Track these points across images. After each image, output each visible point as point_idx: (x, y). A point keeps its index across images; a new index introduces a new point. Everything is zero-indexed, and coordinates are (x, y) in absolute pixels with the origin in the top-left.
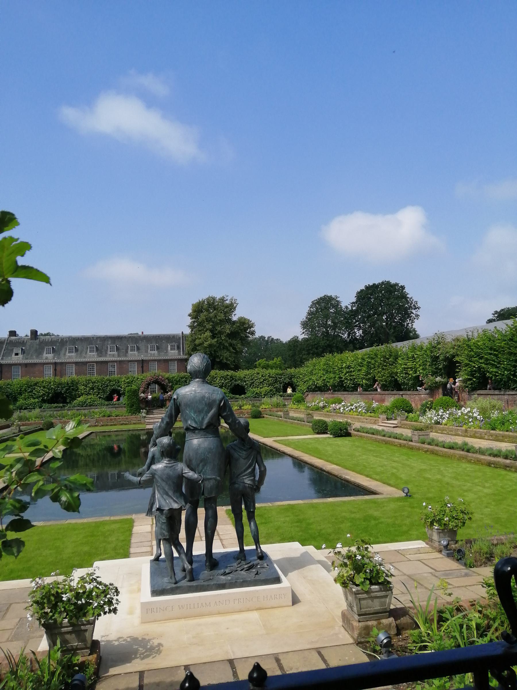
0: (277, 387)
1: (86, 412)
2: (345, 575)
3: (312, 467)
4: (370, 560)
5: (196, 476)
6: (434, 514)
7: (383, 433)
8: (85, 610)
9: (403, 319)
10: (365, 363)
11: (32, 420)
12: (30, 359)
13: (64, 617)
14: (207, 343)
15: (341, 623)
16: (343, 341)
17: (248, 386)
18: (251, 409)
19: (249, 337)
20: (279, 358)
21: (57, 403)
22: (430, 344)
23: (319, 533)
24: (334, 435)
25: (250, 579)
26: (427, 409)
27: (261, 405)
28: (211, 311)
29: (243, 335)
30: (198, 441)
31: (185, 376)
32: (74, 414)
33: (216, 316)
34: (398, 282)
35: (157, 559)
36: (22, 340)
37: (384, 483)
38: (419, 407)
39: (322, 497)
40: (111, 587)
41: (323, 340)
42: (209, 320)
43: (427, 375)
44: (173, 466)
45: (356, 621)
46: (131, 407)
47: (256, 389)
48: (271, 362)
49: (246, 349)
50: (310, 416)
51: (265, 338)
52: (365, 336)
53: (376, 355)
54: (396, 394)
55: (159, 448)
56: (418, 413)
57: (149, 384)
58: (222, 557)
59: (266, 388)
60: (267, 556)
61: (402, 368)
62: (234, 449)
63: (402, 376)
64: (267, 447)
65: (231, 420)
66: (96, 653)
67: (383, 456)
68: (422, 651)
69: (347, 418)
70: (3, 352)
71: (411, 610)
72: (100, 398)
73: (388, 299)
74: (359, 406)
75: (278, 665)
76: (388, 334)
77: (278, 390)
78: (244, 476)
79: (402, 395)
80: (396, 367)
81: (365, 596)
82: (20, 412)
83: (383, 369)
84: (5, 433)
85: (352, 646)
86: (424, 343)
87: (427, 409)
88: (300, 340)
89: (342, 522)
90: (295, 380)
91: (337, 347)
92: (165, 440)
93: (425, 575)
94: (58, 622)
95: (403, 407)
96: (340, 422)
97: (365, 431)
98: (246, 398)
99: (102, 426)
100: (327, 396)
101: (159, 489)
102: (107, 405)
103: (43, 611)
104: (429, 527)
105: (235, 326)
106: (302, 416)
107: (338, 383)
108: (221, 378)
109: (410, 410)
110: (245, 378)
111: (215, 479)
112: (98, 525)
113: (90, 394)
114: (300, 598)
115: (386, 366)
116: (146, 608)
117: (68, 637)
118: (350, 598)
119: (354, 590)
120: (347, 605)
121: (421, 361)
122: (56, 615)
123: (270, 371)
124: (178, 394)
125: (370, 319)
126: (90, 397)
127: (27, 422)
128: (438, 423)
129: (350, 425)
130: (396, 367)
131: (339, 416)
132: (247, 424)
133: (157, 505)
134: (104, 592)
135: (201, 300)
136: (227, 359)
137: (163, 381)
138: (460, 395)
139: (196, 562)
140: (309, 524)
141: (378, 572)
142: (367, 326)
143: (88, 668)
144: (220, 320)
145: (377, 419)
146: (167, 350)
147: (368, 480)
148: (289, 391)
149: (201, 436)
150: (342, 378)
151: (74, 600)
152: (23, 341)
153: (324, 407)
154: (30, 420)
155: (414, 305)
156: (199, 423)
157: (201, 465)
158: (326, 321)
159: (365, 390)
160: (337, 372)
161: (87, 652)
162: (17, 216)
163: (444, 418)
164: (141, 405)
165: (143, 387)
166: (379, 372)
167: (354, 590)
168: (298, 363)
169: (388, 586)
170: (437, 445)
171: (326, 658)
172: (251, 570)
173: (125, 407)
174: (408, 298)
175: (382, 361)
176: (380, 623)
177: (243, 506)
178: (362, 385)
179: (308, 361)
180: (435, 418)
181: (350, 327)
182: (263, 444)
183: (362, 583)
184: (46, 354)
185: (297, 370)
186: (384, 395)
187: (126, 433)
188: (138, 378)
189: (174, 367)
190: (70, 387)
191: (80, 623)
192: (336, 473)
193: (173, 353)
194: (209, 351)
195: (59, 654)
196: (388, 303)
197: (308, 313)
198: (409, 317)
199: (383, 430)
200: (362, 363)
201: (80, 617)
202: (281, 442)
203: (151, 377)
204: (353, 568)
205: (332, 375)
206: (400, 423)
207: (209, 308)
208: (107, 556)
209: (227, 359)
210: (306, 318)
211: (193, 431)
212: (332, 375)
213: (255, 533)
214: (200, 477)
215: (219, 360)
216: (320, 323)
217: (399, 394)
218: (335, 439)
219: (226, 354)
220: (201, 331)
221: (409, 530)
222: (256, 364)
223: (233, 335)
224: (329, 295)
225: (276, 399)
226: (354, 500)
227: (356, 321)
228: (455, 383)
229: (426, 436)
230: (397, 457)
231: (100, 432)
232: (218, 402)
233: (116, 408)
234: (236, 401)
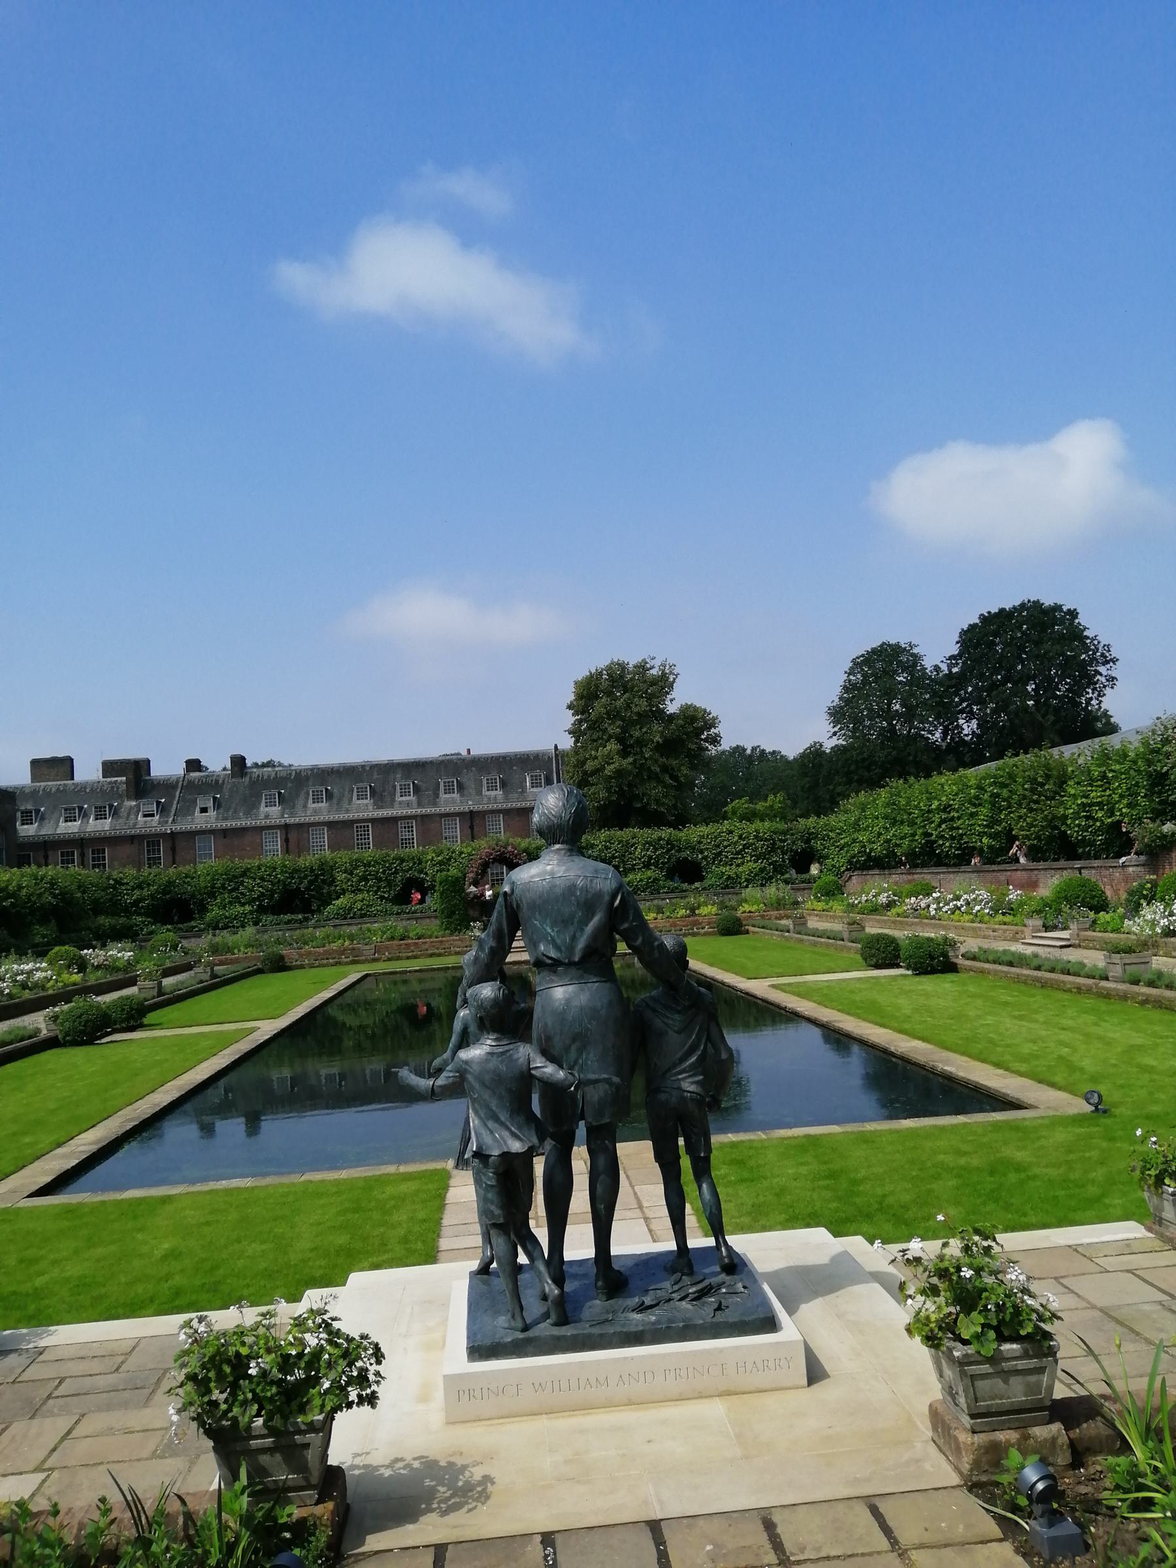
0: (776, 861)
1: (354, 929)
2: (933, 1317)
4: (997, 1279)
5: (561, 1074)
6: (1164, 1156)
7: (1035, 963)
8: (303, 1398)
9: (1077, 689)
10: (986, 796)
11: (239, 951)
12: (233, 818)
13: (254, 1413)
14: (612, 766)
15: (929, 1434)
16: (931, 747)
17: (708, 862)
20: (780, 797)
21: (292, 913)
22: (1145, 743)
23: (880, 1203)
24: (914, 969)
25: (701, 1322)
26: (1142, 901)
27: (740, 903)
28: (618, 694)
29: (694, 747)
30: (565, 992)
32: (328, 936)
33: (628, 707)
37: (1040, 1082)
38: (1124, 896)
39: (891, 1117)
40: (365, 1343)
41: (882, 749)
43: (1140, 819)
44: (507, 1051)
45: (965, 1429)
46: (449, 917)
47: (728, 868)
48: (760, 806)
50: (855, 926)
52: (983, 734)
54: (1066, 869)
55: (473, 1010)
56: (1121, 910)
58: (637, 1265)
59: (750, 866)
61: (1078, 805)
62: (654, 1010)
63: (1079, 825)
65: (640, 940)
66: (331, 1498)
67: (1037, 1016)
68: (1140, 1511)
69: (944, 927)
70: (174, 806)
71: (1107, 1404)
72: (382, 898)
74: (975, 899)
75: (770, 1540)
78: (680, 1073)
79: (1080, 869)
81: (986, 1368)
82: (214, 935)
83: (1031, 810)
84: (182, 983)
85: (957, 1492)
86: (1130, 743)
87: (1142, 901)
88: (828, 751)
89: (937, 1177)
90: (818, 845)
92: (487, 991)
93: (1147, 1307)
94: (241, 1425)
95: (1083, 899)
96: (930, 939)
97: (991, 958)
98: (704, 889)
99: (389, 959)
100: (897, 878)
102: (398, 914)
103: (206, 1399)
104: (1152, 1189)
105: (673, 726)
106: (837, 926)
108: (644, 845)
109: (1102, 905)
110: (700, 842)
111: (607, 1081)
112: (370, 1184)
113: (360, 890)
114: (828, 1366)
116: (457, 1387)
117: (264, 1459)
118: (948, 1373)
119: (956, 1354)
120: (943, 1388)
122: (236, 1410)
123: (757, 824)
124: (513, 883)
125: (994, 693)
126: (360, 896)
127: (229, 956)
129: (953, 944)
130: (1062, 803)
131: (927, 925)
134: (346, 1354)
135: (593, 671)
136: (657, 801)
137: (516, 856)
139: (575, 1276)
140: (855, 1182)
141: (1017, 1311)
142: (988, 711)
143: (314, 1534)
144: (638, 714)
145: (1020, 928)
146: (524, 791)
149: (571, 980)
150: (931, 835)
151: (276, 1374)
152: (217, 781)
153: (890, 905)
154: (236, 951)
155: (1103, 655)
157: (574, 1048)
158: (889, 704)
159: (990, 861)
160: (918, 821)
161: (310, 1496)
164: (471, 913)
166: (1020, 817)
167: (956, 1354)
168: (824, 805)
169: (1046, 1344)
171: (890, 1523)
172: (704, 1299)
173: (436, 917)
174: (1087, 638)
175: (1026, 790)
176: (1026, 1437)
177: (681, 1141)
178: (981, 849)
179: (848, 800)
181: (946, 714)
182: (747, 994)
183: (978, 1337)
184: (266, 806)
185: (823, 820)
186: (1036, 872)
187: (442, 974)
188: (461, 853)
190: (317, 876)
191: (291, 1429)
192: (921, 1059)
194: (616, 786)
195: (245, 1499)
197: (845, 687)
198: (1091, 682)
199: (1036, 956)
200: (977, 797)
201: (291, 1413)
202: (787, 989)
204: (954, 1301)
205: (907, 830)
206: (1078, 935)
208: (385, 1257)
209: (657, 801)
212: (907, 830)
213: (714, 1210)
214: (570, 1077)
215: (639, 805)
216: (873, 710)
217: (1072, 868)
218: (918, 979)
219: (656, 791)
221: (1103, 1195)
222: (726, 812)
223: (670, 747)
224: (893, 642)
226: (965, 1125)
227: (962, 700)
230: (1072, 1018)
231: (384, 974)
232: (607, 898)
233: (416, 919)
234: (682, 898)
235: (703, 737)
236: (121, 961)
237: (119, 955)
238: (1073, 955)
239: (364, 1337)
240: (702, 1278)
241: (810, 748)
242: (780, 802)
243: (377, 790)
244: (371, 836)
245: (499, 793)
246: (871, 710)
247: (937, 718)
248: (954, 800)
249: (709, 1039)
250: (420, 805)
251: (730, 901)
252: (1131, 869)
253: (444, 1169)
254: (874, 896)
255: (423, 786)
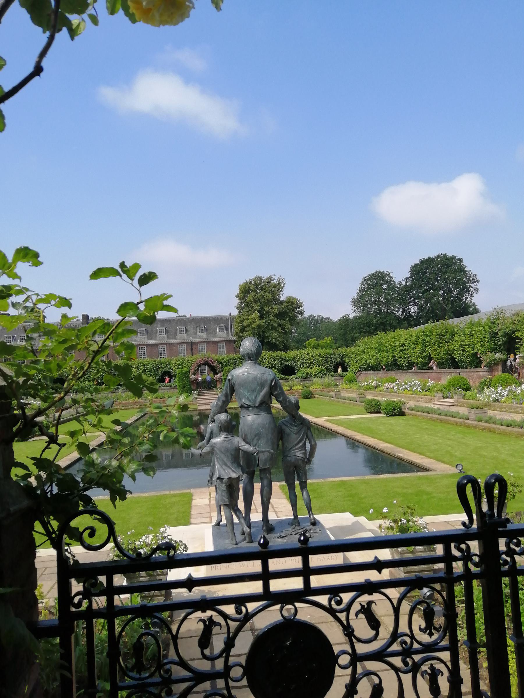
0: (328, 367)
3: (366, 446)
7: (439, 412)
10: (420, 340)
14: (255, 323)
18: (301, 389)
19: (298, 317)
20: (330, 338)
22: (488, 319)
24: (387, 414)
27: (312, 385)
28: (259, 291)
29: (292, 315)
31: (234, 357)
32: (128, 396)
34: (455, 255)
35: (218, 524)
36: (74, 324)
37: (438, 461)
38: (478, 384)
39: (374, 474)
42: (257, 301)
43: (485, 351)
47: (307, 369)
48: (321, 342)
49: (295, 329)
51: (315, 317)
53: (431, 332)
56: (476, 391)
57: (199, 366)
60: (319, 523)
61: (459, 345)
62: (286, 425)
63: (459, 354)
64: (318, 426)
65: (282, 398)
69: (401, 397)
73: (444, 273)
74: (414, 385)
76: (445, 309)
77: (328, 370)
78: (296, 449)
79: (459, 373)
80: (452, 344)
83: (439, 347)
86: (482, 319)
88: (351, 318)
90: (346, 360)
91: (390, 325)
92: (223, 417)
96: (393, 401)
98: (296, 378)
100: (381, 375)
101: (218, 460)
105: (283, 306)
106: (354, 396)
107: (391, 362)
109: (468, 388)
110: (294, 358)
111: (269, 452)
115: (441, 343)
121: (479, 337)
123: (320, 350)
128: (496, 401)
129: (404, 404)
130: (452, 344)
132: (298, 403)
133: (217, 475)
135: (248, 280)
136: (275, 339)
138: (520, 372)
139: (254, 527)
142: (422, 302)
144: (268, 300)
145: (432, 397)
146: (215, 332)
147: (421, 458)
148: (340, 370)
149: (255, 413)
150: (395, 356)
153: (377, 387)
155: (473, 279)
156: (252, 401)
158: (379, 298)
160: (390, 350)
161: (162, 599)
162: (157, 274)
163: (503, 396)
164: (192, 387)
165: (193, 369)
166: (434, 350)
168: (349, 342)
170: (494, 423)
173: (177, 389)
174: (466, 271)
175: (437, 338)
178: (417, 363)
180: (494, 396)
181: (404, 303)
185: (349, 349)
186: (440, 373)
188: (188, 360)
189: (223, 348)
192: (389, 451)
193: (221, 335)
196: (444, 277)
197: (360, 290)
199: (439, 409)
202: (332, 422)
203: (201, 359)
206: (457, 401)
207: (257, 288)
210: (357, 295)
211: (248, 409)
212: (385, 354)
215: (267, 341)
216: (372, 301)
220: (248, 312)
223: (281, 315)
224: (381, 271)
225: (327, 379)
226: (406, 477)
227: (411, 297)
228: (515, 359)
229: (483, 414)
230: (452, 435)
232: (269, 382)
235: (296, 311)
236: (36, 405)
237: (35, 403)
238: (454, 409)
239: (180, 541)
240: (303, 527)
241: (343, 317)
242: (330, 341)
243: (149, 331)
244: (146, 352)
245: (205, 334)
246: (371, 301)
247: (400, 304)
248: (406, 342)
249: (307, 437)
250: (168, 338)
251: (307, 383)
252: (481, 373)
253: (190, 493)
254: (370, 383)
255: (170, 330)
